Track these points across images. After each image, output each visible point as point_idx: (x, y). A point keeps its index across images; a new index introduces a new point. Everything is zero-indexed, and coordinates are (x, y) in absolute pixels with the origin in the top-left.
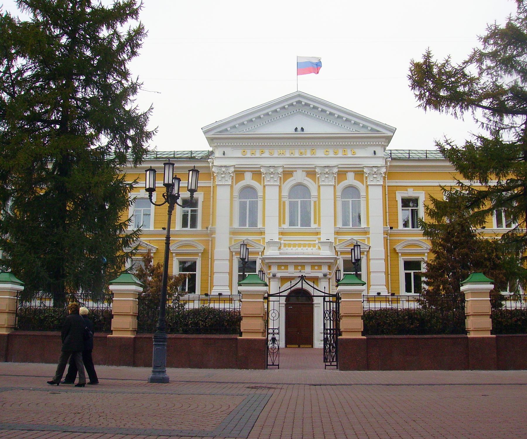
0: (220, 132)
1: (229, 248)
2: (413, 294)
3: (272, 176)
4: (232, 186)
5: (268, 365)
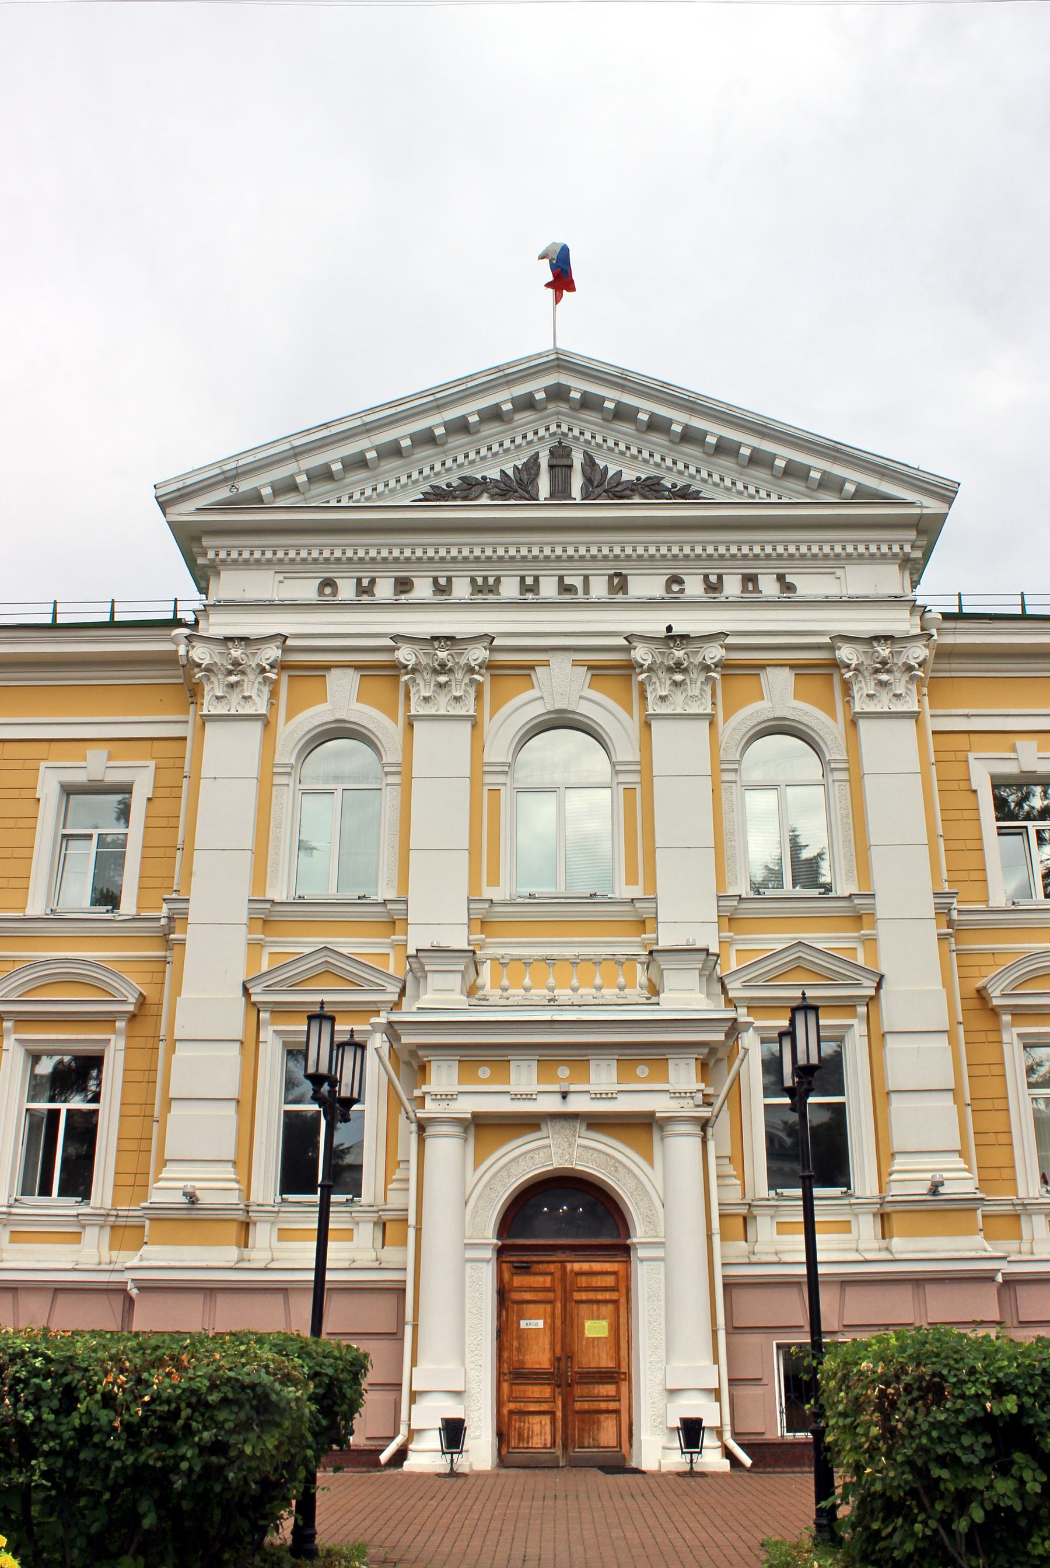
1: (246, 991)
3: (443, 679)
4: (267, 722)
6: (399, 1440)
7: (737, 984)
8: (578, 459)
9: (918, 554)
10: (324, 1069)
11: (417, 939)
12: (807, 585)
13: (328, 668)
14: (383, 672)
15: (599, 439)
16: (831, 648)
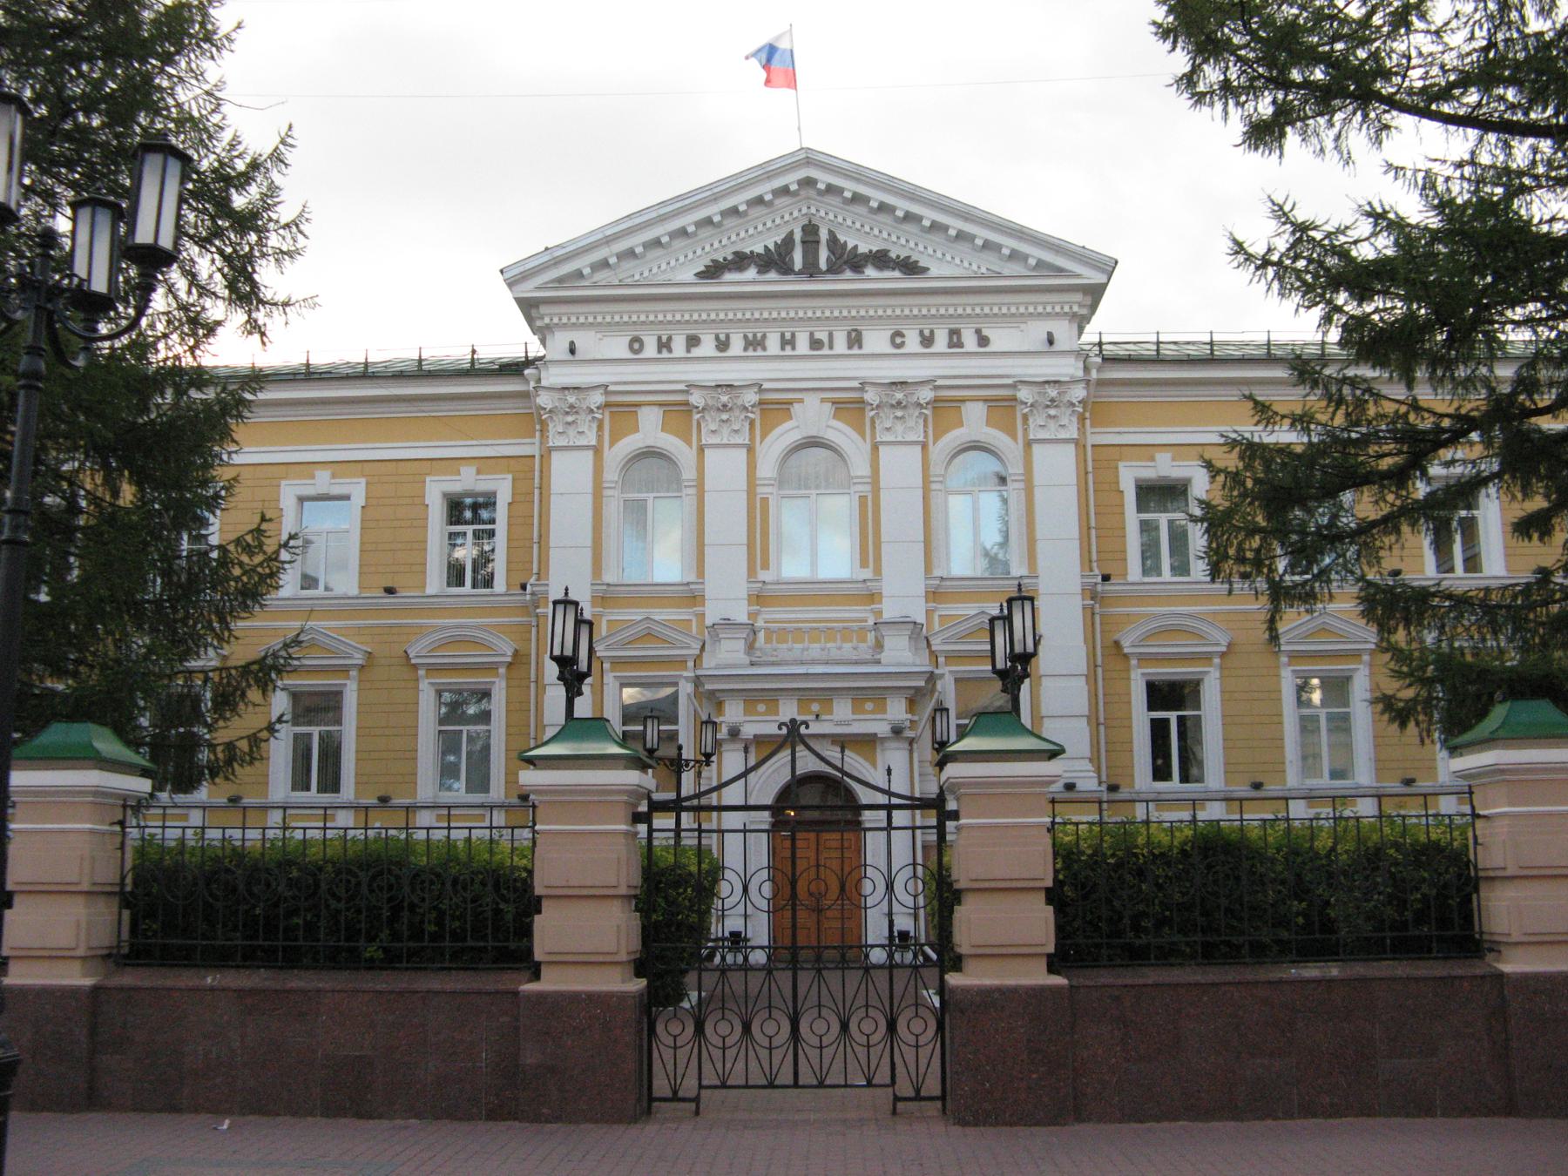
0: (560, 280)
2: (1174, 784)
3: (725, 417)
5: (651, 1099)
7: (938, 641)
8: (824, 235)
9: (1084, 311)
11: (712, 614)
12: (1001, 339)
13: (963, 401)
14: (679, 412)
15: (840, 219)
16: (1014, 386)
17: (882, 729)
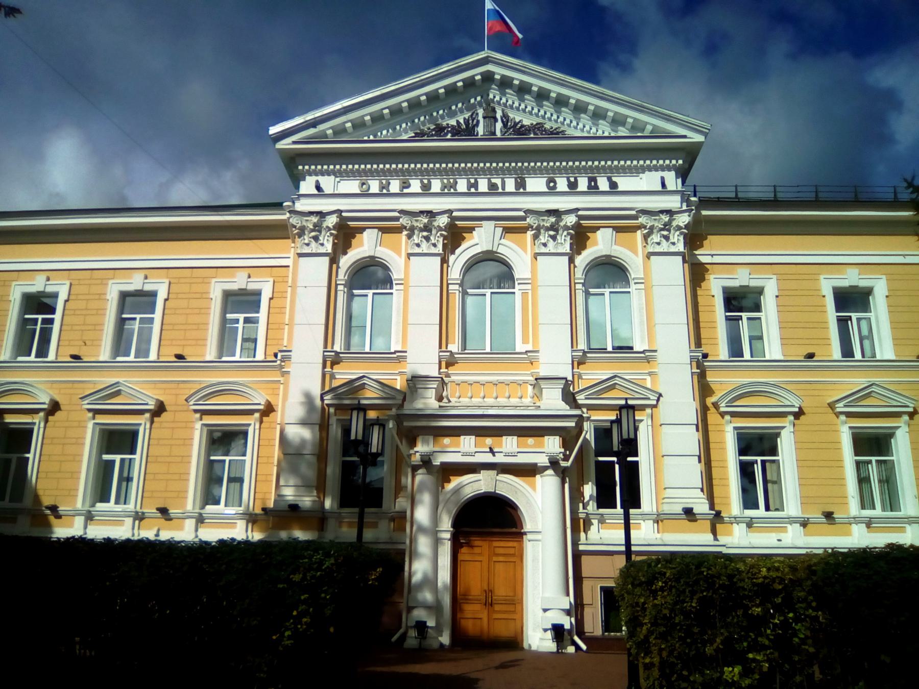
2: (761, 512)
6: (402, 631)
10: (360, 437)
12: (624, 183)
13: (598, 228)
17: (543, 460)
